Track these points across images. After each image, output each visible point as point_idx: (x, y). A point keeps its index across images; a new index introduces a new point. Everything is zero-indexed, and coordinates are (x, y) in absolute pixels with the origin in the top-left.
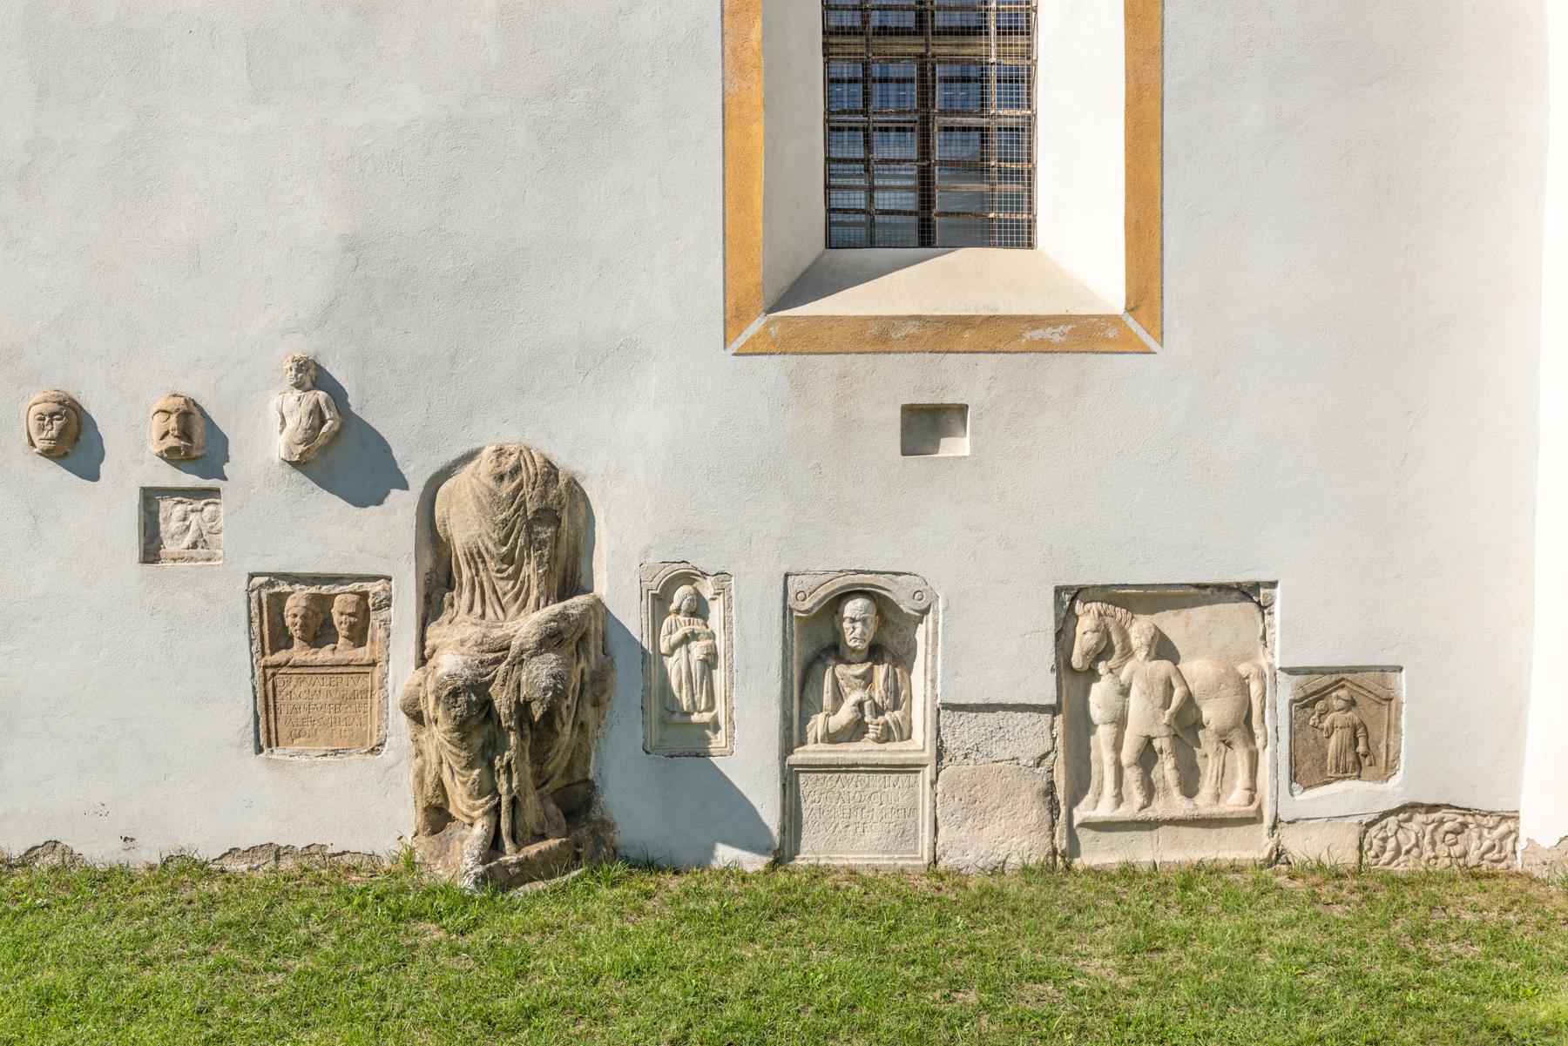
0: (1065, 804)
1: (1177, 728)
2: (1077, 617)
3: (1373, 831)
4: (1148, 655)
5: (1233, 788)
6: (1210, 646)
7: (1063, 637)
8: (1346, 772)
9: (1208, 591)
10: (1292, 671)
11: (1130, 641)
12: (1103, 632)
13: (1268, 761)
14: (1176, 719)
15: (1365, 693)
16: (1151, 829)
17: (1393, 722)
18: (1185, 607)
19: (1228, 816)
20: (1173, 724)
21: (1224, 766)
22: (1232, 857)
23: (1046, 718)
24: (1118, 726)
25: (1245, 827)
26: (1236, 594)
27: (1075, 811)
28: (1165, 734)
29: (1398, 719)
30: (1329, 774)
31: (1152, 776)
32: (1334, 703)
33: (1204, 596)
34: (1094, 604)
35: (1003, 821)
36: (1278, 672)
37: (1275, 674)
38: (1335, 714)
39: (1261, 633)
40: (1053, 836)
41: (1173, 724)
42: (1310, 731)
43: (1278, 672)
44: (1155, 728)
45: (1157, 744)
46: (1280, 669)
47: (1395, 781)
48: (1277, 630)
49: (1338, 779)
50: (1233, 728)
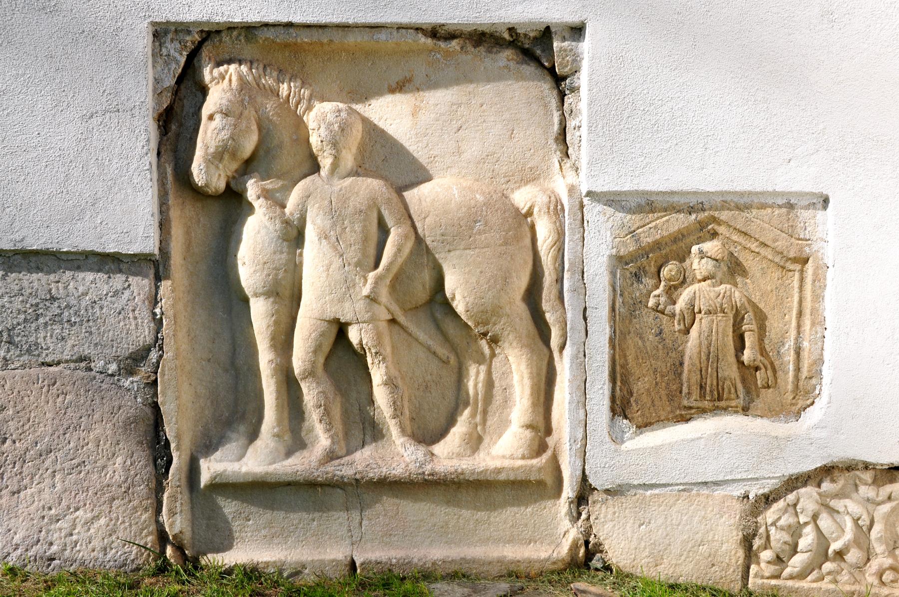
1: (395, 308)
3: (770, 515)
5: (505, 423)
6: (459, 152)
8: (720, 398)
10: (612, 200)
15: (754, 246)
17: (808, 305)
19: (491, 478)
23: (140, 285)
29: (818, 297)
30: (685, 403)
32: (695, 266)
34: (233, 67)
35: (58, 477)
36: (586, 201)
37: (582, 206)
38: (696, 287)
40: (158, 510)
42: (649, 318)
43: (586, 201)
45: (354, 334)
46: (589, 194)
47: (813, 415)
49: (703, 411)
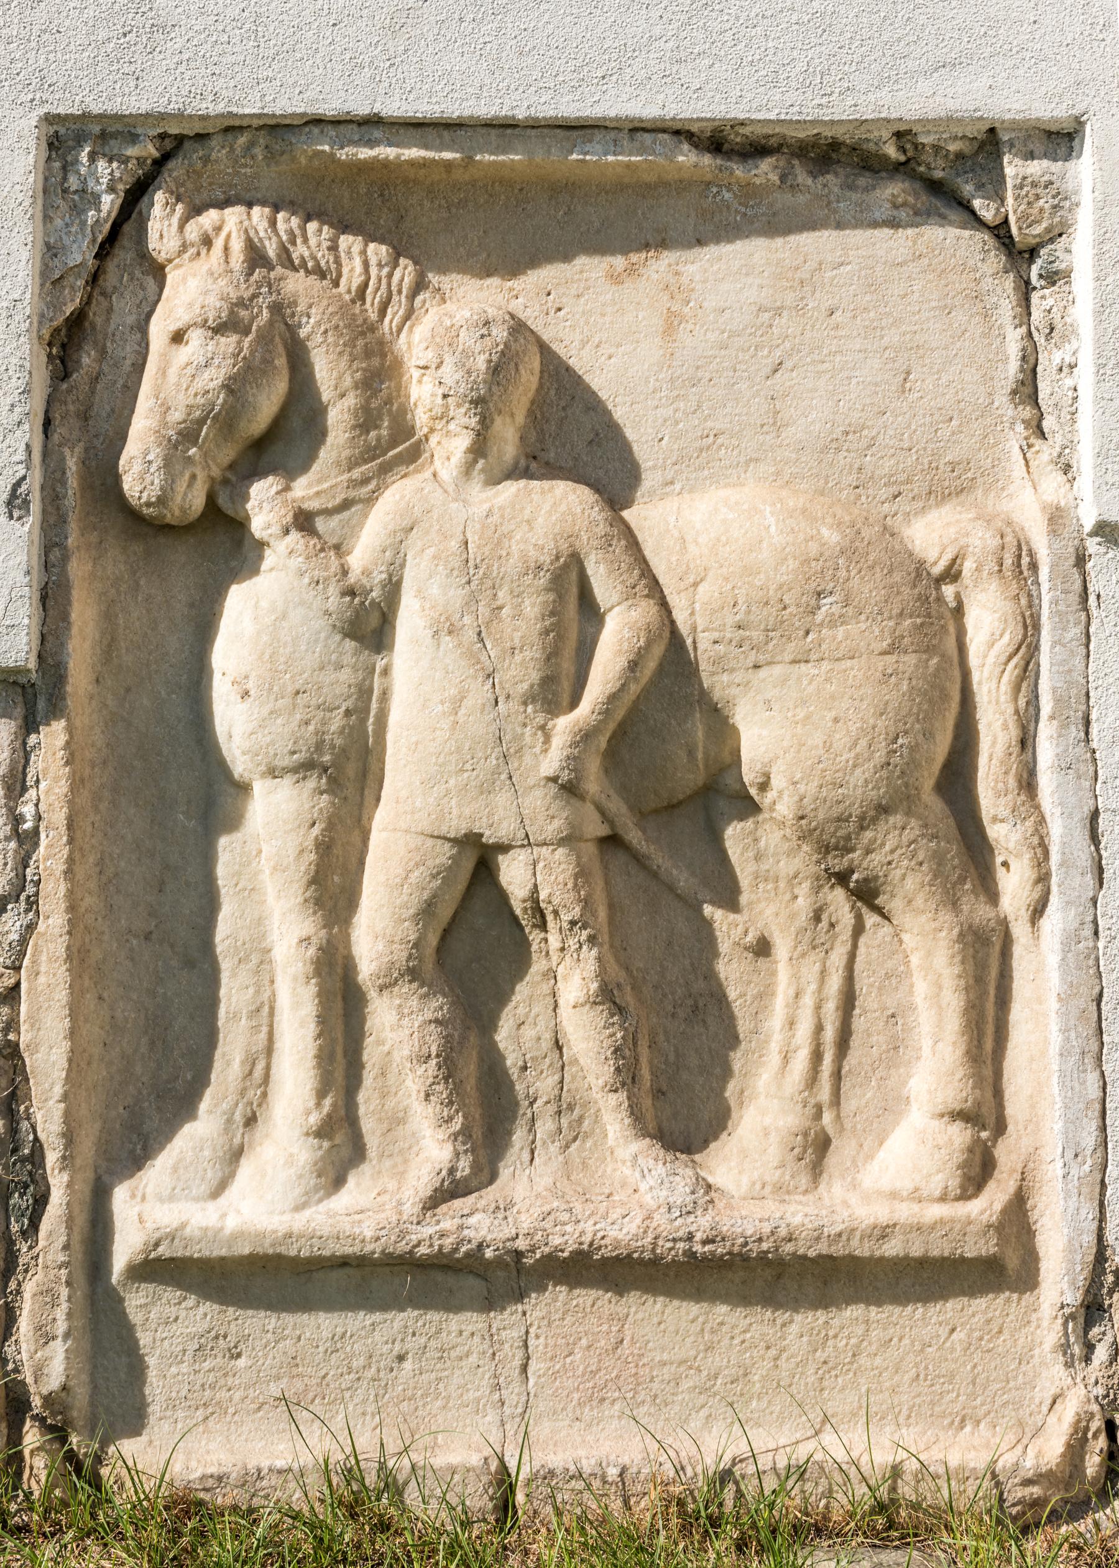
0: (66, 1161)
1: (617, 806)
2: (158, 272)
4: (479, 449)
6: (776, 423)
7: (87, 359)
9: (766, 170)
11: (400, 390)
12: (264, 339)
13: (1054, 980)
14: (613, 757)
16: (490, 1303)
18: (661, 242)
19: (863, 1250)
20: (593, 785)
21: (849, 1000)
22: (884, 1457)
24: (334, 785)
25: (952, 1306)
26: (895, 189)
27: (121, 1196)
28: (554, 827)
31: (503, 1036)
33: (748, 192)
34: (233, 215)
36: (1093, 545)
37: (1081, 560)
39: (1013, 367)
41: (593, 785)
43: (1093, 545)
44: (502, 799)
48: (1085, 377)
50: (884, 809)
